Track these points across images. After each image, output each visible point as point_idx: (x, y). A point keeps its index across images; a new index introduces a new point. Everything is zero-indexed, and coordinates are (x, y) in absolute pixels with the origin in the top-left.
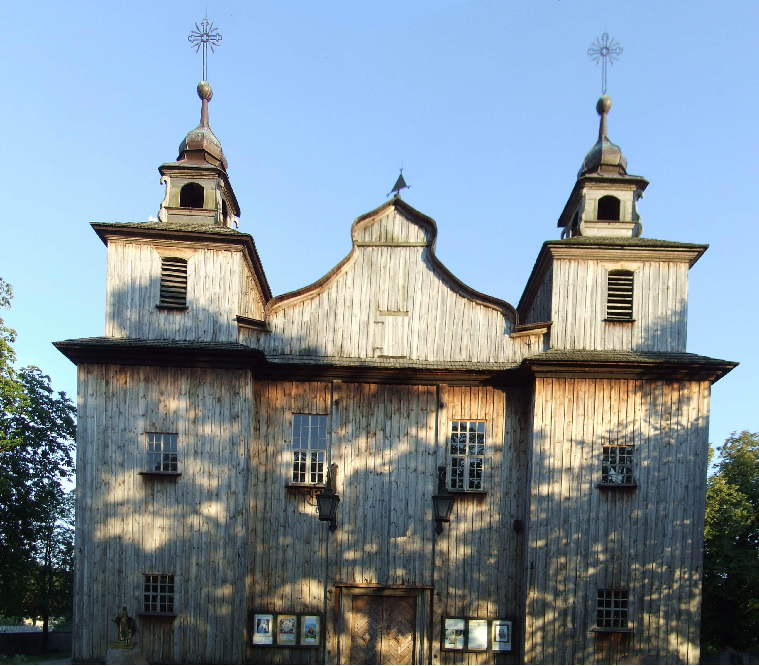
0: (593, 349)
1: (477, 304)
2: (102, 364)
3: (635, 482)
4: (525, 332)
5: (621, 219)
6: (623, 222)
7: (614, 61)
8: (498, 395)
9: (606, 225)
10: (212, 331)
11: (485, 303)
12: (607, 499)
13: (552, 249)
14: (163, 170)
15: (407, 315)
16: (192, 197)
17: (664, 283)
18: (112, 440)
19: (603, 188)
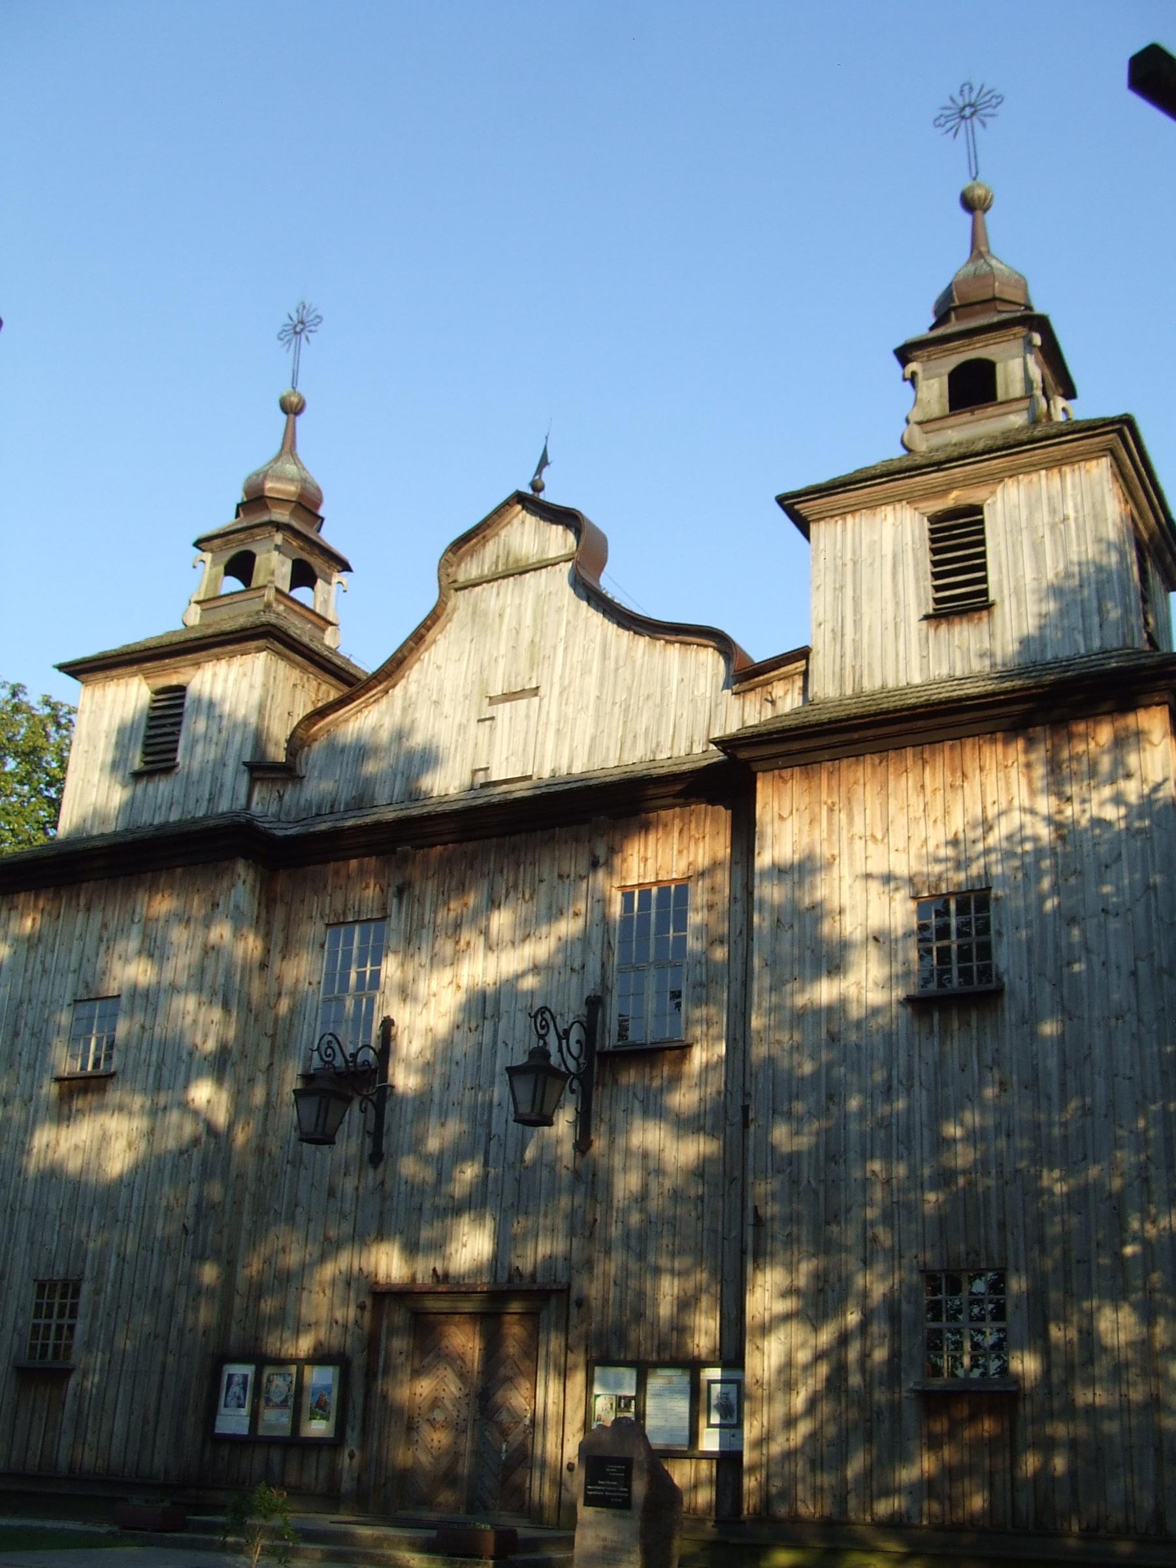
0: (903, 684)
1: (667, 642)
2: (30, 890)
3: (999, 978)
4: (761, 678)
5: (1001, 395)
6: (1002, 403)
7: (988, 120)
8: (715, 820)
9: (966, 417)
10: (207, 796)
11: (680, 637)
12: (931, 1032)
13: (797, 507)
14: (904, 354)
15: (536, 695)
16: (972, 388)
17: (1053, 511)
18: (26, 1024)
19: (954, 351)
